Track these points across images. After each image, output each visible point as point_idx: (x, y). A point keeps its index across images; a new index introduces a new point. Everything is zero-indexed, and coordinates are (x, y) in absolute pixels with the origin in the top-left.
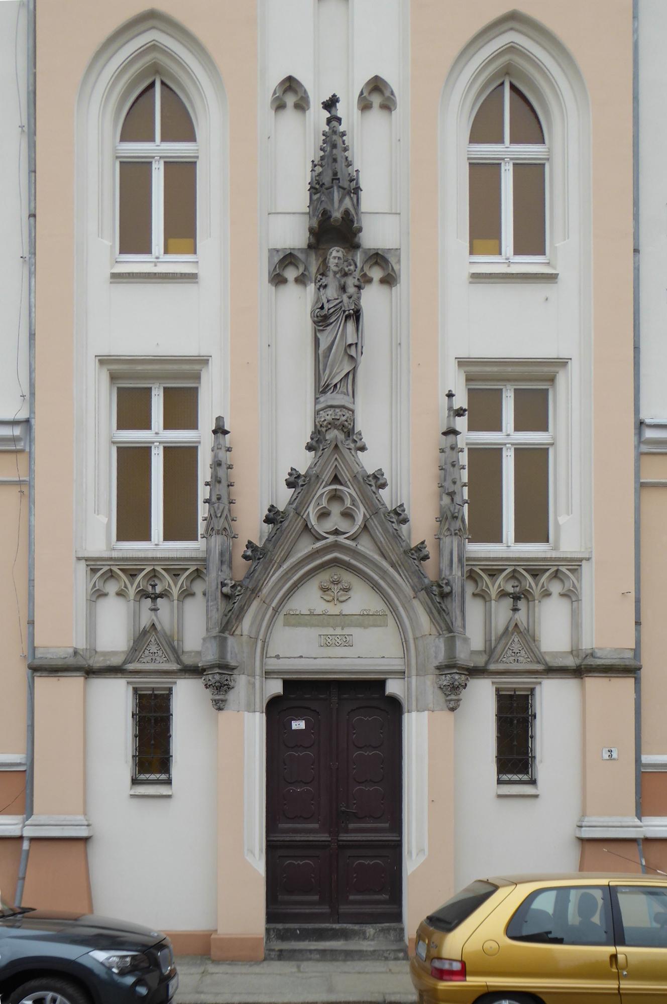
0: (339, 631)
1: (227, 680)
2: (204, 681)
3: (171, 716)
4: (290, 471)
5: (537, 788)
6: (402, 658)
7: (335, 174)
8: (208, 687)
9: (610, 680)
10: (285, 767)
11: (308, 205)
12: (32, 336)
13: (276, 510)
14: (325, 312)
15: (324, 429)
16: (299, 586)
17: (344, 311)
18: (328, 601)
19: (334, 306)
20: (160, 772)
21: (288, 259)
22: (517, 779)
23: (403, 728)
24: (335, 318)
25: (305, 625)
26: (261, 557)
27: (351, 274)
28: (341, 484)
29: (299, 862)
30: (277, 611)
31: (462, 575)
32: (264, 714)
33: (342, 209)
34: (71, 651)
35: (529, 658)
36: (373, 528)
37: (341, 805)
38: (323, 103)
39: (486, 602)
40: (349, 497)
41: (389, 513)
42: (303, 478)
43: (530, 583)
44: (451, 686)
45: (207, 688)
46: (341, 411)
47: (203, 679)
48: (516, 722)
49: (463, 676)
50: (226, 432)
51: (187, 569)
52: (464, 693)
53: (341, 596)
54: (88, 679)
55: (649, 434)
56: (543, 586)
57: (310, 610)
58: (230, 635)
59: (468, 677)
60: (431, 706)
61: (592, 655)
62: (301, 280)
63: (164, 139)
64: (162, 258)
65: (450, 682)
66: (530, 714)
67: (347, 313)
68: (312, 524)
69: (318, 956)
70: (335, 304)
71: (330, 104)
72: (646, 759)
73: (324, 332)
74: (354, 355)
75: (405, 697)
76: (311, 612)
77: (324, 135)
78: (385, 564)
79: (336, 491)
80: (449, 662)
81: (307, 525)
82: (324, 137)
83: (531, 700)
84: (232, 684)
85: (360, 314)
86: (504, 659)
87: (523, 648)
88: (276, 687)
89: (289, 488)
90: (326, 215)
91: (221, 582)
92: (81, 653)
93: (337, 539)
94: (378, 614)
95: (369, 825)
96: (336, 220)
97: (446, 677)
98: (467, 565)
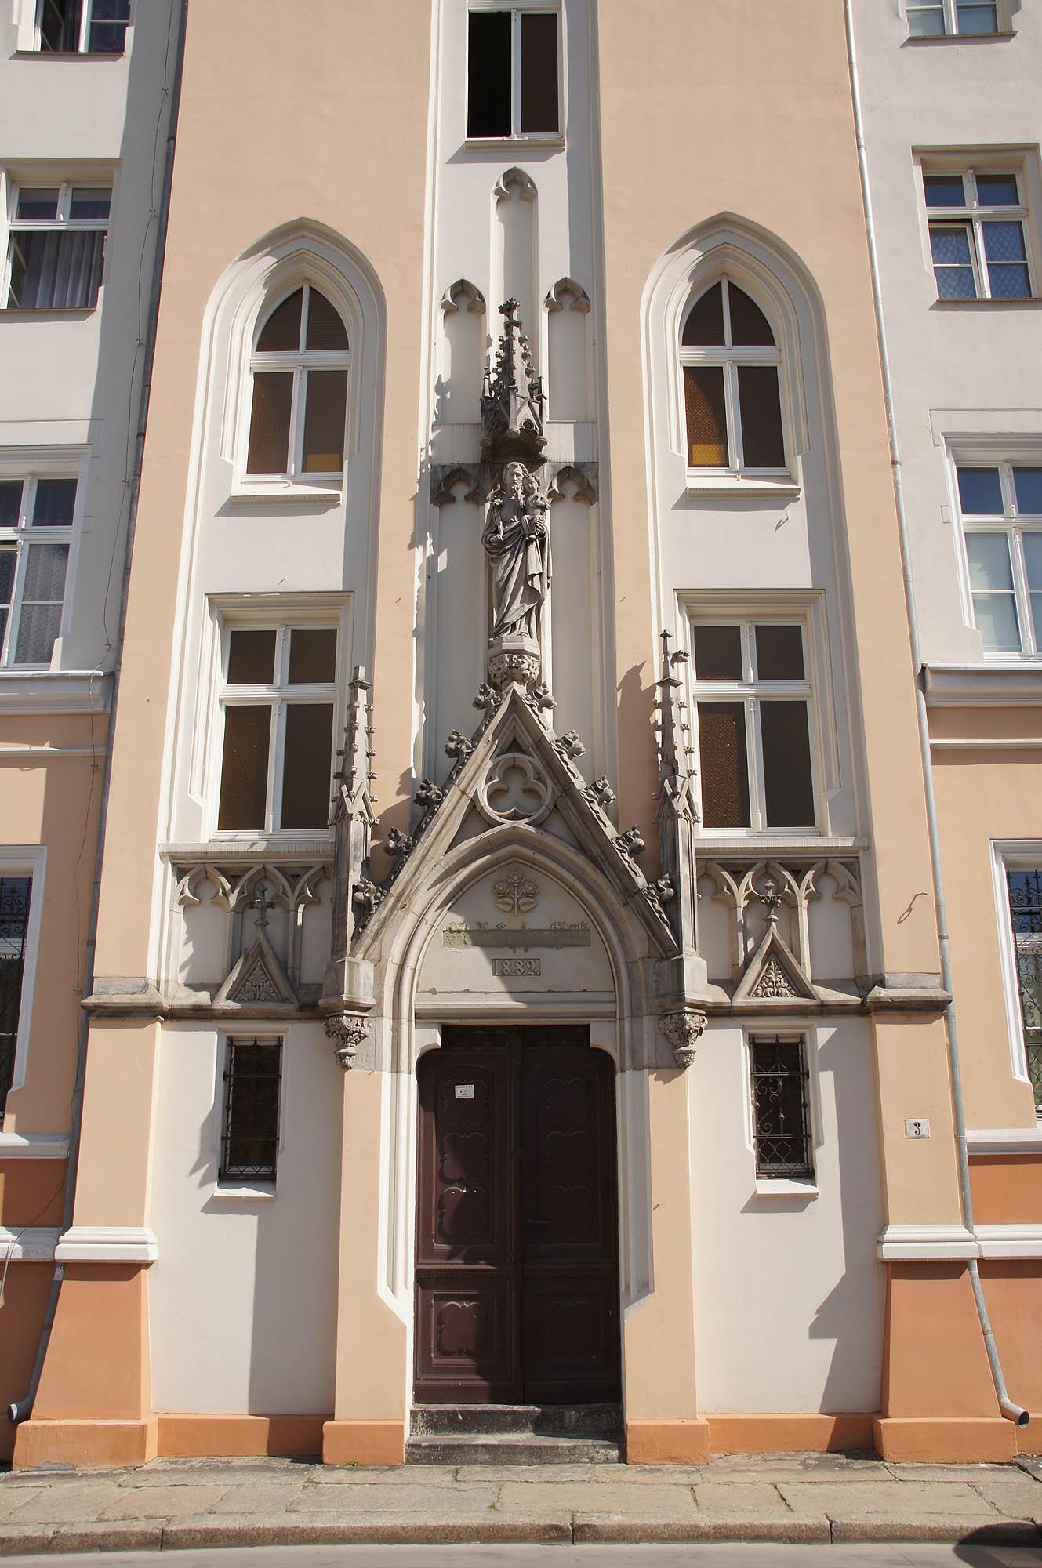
0: (520, 953)
1: (357, 1025)
5: (814, 1184)
15: (498, 681)
16: (464, 890)
28: (522, 751)
48: (781, 1083)
51: (311, 868)
53: (524, 904)
57: (479, 924)
79: (514, 761)
81: (475, 806)
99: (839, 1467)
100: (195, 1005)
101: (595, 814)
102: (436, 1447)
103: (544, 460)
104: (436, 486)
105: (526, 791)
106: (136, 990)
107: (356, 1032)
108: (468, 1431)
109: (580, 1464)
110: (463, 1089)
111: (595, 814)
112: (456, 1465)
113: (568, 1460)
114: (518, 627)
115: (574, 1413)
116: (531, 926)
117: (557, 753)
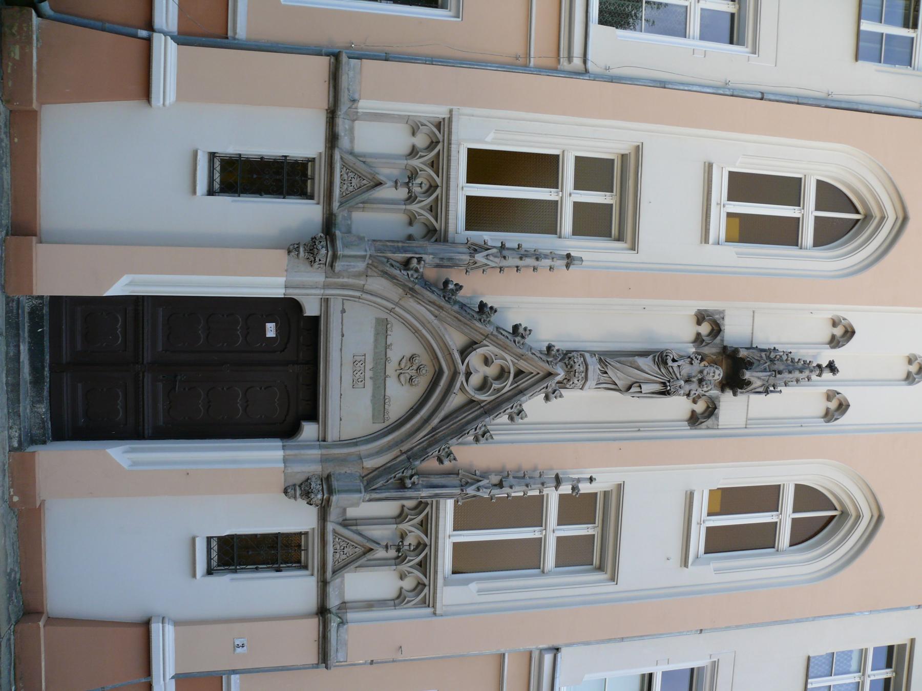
0: (369, 374)
1: (320, 260)
2: (319, 235)
3: (282, 197)
4: (529, 328)
6: (340, 438)
7: (780, 372)
8: (314, 240)
9: (316, 641)
10: (225, 316)
11: (759, 347)
12: (663, 84)
13: (492, 315)
14: (670, 363)
15: (566, 361)
16: (416, 334)
17: (669, 381)
18: (399, 364)
19: (674, 372)
20: (222, 182)
21: (717, 330)
22: (212, 555)
23: (266, 439)
24: (664, 373)
25: (376, 340)
26: (446, 299)
27: (700, 387)
28: (515, 377)
29: (119, 330)
30: (391, 311)
31: (422, 498)
32: (283, 296)
33: (752, 379)
34: (356, 97)
35: (339, 563)
36: (471, 408)
37: (183, 375)
38: (833, 361)
39: (395, 518)
40: (502, 385)
41: (485, 426)
42: (490, 329)
43: (412, 560)
44: (310, 491)
45: (312, 239)
46: (582, 378)
47: (322, 235)
48: (273, 552)
49: (320, 502)
50: (568, 266)
51: (437, 220)
52: (302, 503)
54: (326, 112)
55: (548, 658)
56: (409, 573)
57: (391, 344)
58: (368, 264)
59: (320, 506)
60: (289, 470)
61: (342, 623)
62: (698, 340)
63: (817, 219)
64: (723, 210)
65: (314, 490)
66: (281, 566)
67: (668, 384)
68: (477, 349)
69: (12, 354)
70: (676, 372)
71: (832, 367)
72: (235, 678)
73: (653, 363)
74: (631, 391)
75: (299, 442)
76: (389, 346)
77: (810, 362)
78: (435, 421)
80: (335, 489)
82: (808, 362)
83: (295, 567)
84: (316, 265)
85: (666, 395)
86: (337, 539)
87: (348, 557)
88: (311, 309)
89: (513, 327)
90: (748, 364)
91: (422, 258)
92: (354, 106)
93: (461, 374)
94: (385, 414)
95: (160, 406)
96: (743, 374)
97: (320, 485)
98: (432, 501)
99: (10, 596)
100: (338, 135)
101: (466, 432)
102: (18, 318)
103: (723, 390)
104: (710, 313)
105: (485, 379)
106: (351, 92)
107: (315, 260)
108: (30, 336)
109: (7, 420)
110: (272, 329)
111: (466, 432)
112: (6, 332)
113: (10, 411)
114: (605, 375)
115: (44, 410)
116: (389, 382)
117: (512, 405)
